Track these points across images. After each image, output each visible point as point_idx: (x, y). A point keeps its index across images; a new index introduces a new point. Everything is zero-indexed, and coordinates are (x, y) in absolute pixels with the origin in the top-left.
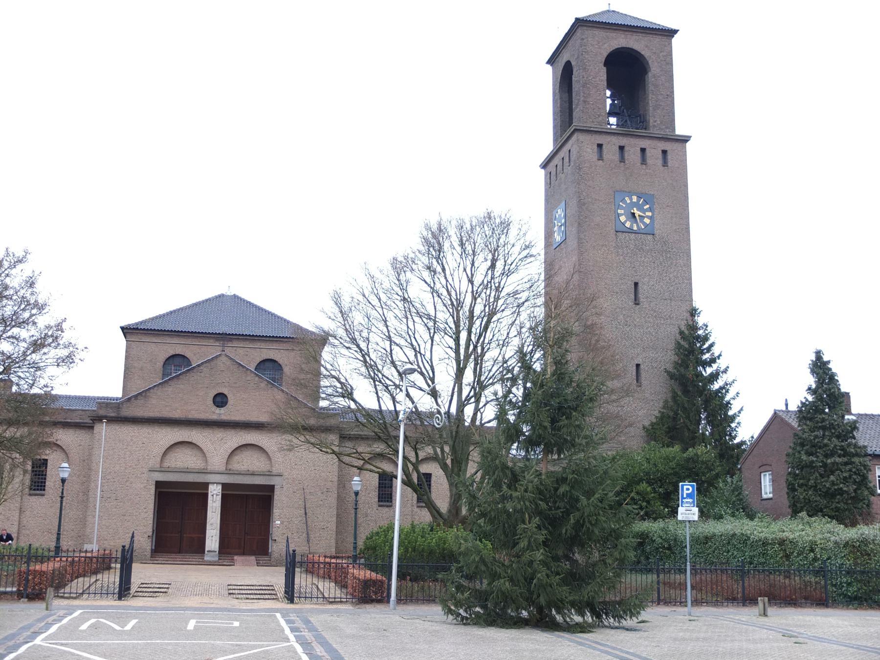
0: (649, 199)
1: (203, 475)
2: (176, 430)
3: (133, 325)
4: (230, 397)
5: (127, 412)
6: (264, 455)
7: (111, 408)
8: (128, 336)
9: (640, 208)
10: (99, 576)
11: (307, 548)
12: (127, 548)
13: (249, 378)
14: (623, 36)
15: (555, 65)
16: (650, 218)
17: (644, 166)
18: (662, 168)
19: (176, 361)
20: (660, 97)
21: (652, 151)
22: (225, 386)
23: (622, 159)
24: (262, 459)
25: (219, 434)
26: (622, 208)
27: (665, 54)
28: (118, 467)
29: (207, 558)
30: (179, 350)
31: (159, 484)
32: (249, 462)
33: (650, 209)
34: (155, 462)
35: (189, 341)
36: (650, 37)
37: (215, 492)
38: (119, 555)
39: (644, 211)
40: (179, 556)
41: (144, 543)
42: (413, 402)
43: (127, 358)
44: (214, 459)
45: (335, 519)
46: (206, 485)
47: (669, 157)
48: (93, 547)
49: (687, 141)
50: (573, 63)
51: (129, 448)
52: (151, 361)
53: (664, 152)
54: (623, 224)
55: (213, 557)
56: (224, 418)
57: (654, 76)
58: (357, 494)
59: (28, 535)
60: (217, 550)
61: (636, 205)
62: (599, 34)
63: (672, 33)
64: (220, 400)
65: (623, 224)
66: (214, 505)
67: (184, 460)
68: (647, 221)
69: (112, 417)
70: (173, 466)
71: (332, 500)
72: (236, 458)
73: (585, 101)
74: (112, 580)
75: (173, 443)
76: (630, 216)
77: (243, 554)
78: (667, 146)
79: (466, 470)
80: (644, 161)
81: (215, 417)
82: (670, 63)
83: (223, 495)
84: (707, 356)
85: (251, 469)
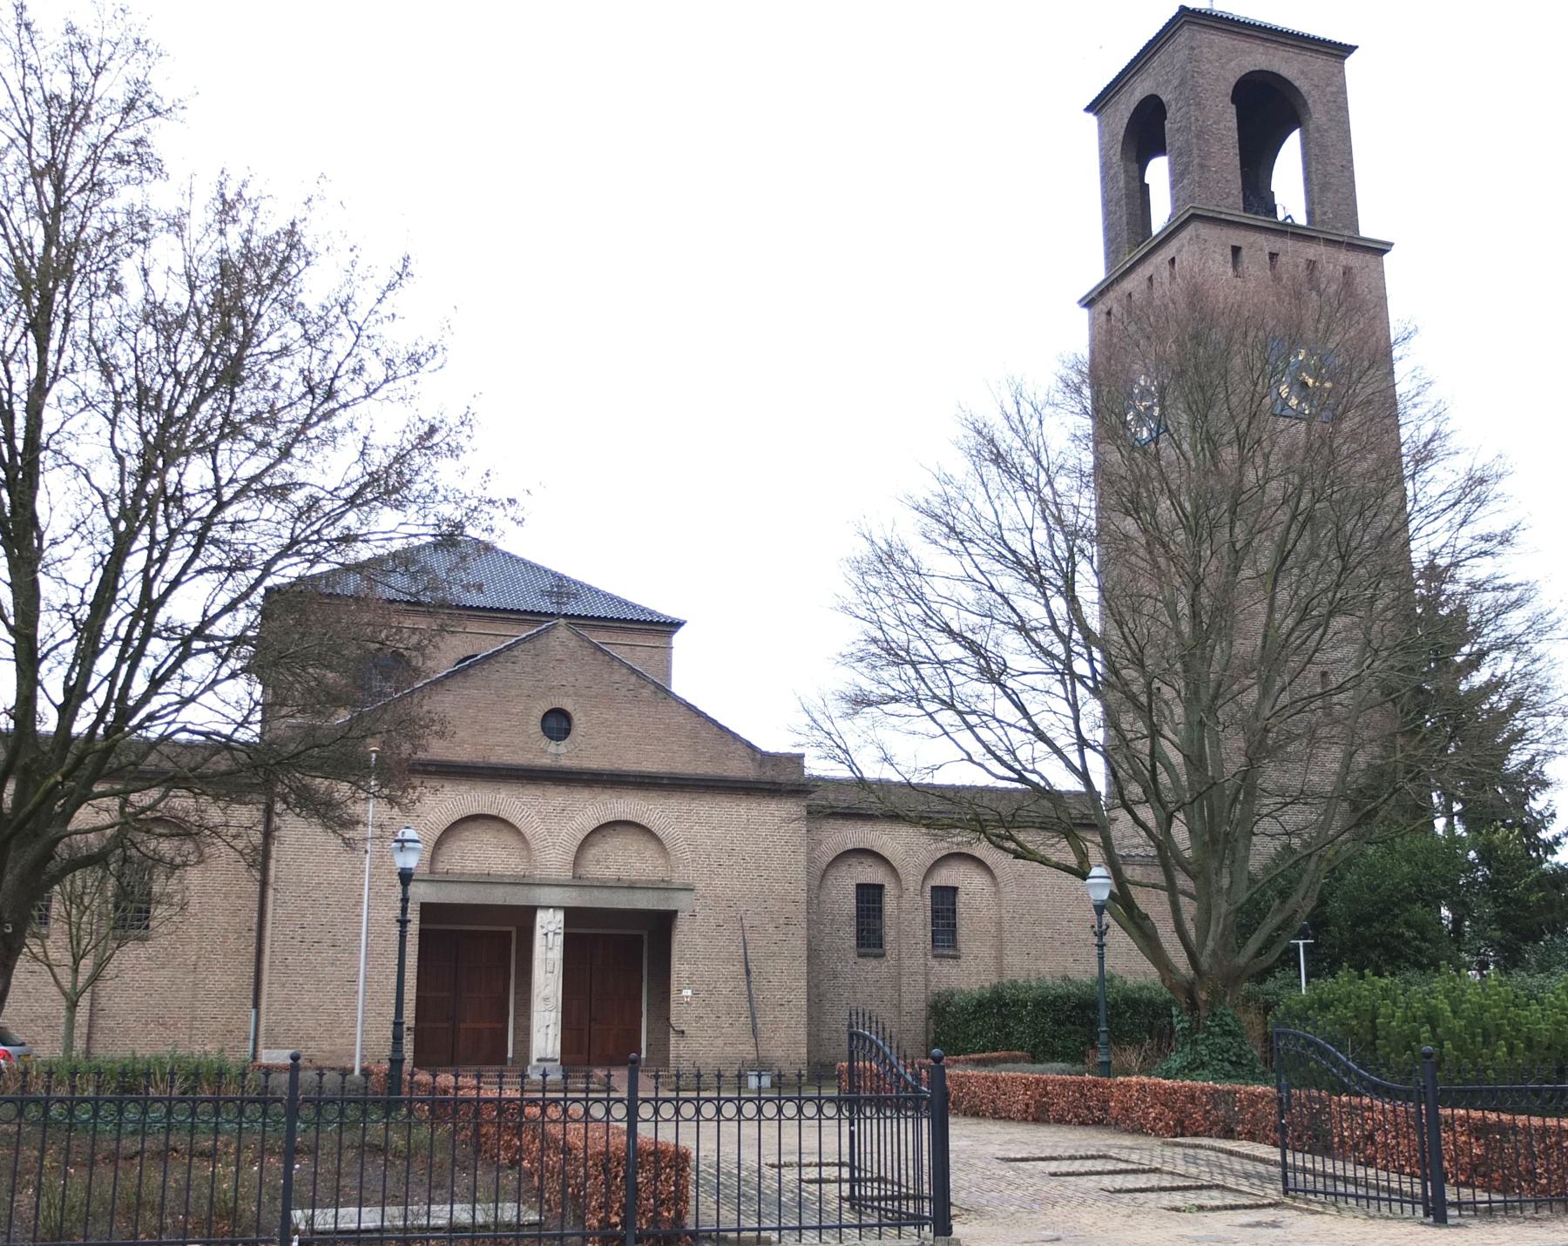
4: (579, 719)
6: (652, 846)
13: (616, 677)
14: (1261, 49)
15: (1109, 111)
22: (567, 695)
24: (647, 854)
25: (557, 798)
27: (1334, 89)
32: (622, 860)
37: (552, 927)
45: (803, 983)
46: (530, 912)
56: (565, 762)
57: (1318, 129)
59: (111, 1029)
60: (558, 1056)
62: (1221, 41)
63: (1350, 49)
64: (557, 724)
66: (550, 955)
67: (482, 855)
70: (457, 869)
71: (799, 945)
72: (593, 853)
73: (1202, 166)
75: (457, 817)
79: (1246, 859)
81: (546, 761)
85: (624, 875)
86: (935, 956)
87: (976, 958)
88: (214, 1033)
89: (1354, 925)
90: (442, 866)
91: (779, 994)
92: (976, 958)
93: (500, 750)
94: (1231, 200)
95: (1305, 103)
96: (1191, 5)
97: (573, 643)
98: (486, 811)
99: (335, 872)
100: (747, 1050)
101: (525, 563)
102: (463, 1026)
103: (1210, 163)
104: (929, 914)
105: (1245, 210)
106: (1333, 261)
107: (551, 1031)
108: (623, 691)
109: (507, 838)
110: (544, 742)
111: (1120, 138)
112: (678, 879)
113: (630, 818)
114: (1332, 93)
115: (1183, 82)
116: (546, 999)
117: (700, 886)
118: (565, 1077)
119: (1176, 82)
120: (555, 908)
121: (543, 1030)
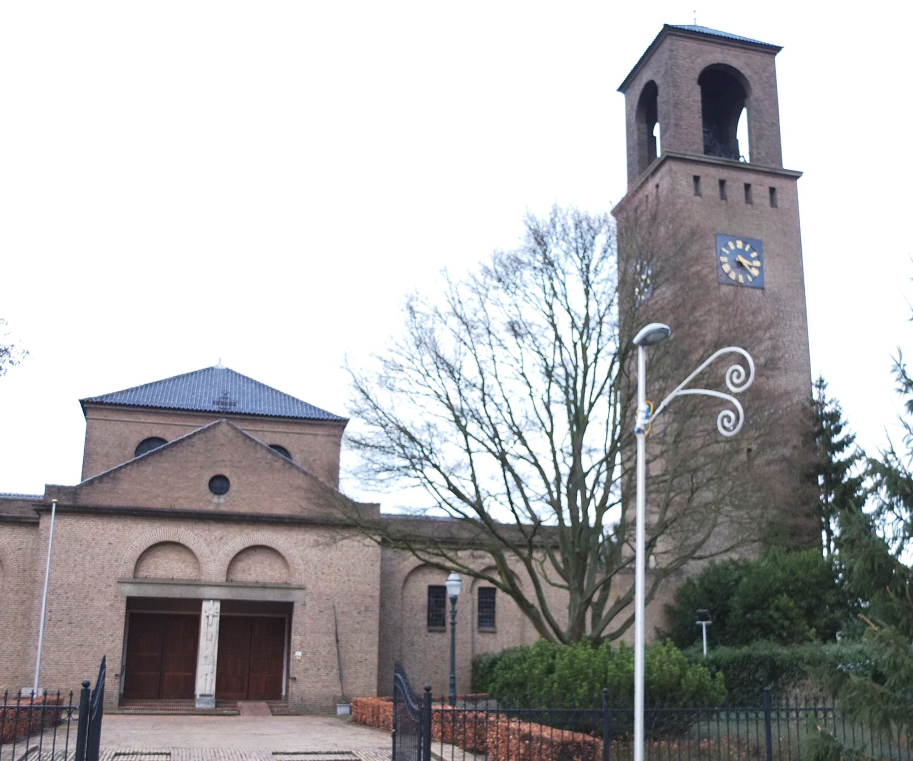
0: (757, 245)
1: (194, 589)
2: (156, 525)
3: (96, 398)
4: (233, 480)
5: (86, 500)
6: (279, 561)
7: (65, 494)
8: (89, 413)
9: (747, 256)
10: (34, 742)
11: (338, 689)
12: (92, 687)
13: (258, 455)
14: (719, 50)
15: (629, 90)
16: (760, 269)
17: (749, 206)
18: (770, 208)
19: (150, 446)
20: (764, 125)
21: (759, 188)
22: (225, 466)
23: (723, 196)
25: (217, 531)
26: (725, 255)
27: (767, 74)
28: (73, 577)
29: (198, 705)
30: (157, 432)
31: (132, 602)
32: (258, 570)
33: (758, 258)
34: (126, 569)
35: (170, 420)
36: (750, 54)
37: (212, 612)
38: (76, 703)
39: (751, 260)
40: (158, 703)
41: (113, 687)
42: (505, 476)
43: (87, 440)
44: (208, 565)
46: (197, 604)
47: (778, 196)
48: (35, 690)
49: (798, 177)
50: (658, 82)
51: (90, 550)
52: (119, 445)
53: (772, 190)
54: (727, 274)
55: (208, 703)
56: (224, 509)
57: (756, 100)
58: (454, 600)
61: (742, 252)
63: (778, 49)
64: (219, 484)
65: (727, 274)
66: (210, 629)
67: (168, 567)
68: (755, 272)
69: (65, 506)
70: (152, 575)
71: (374, 624)
72: (241, 565)
73: (676, 125)
74: (60, 747)
75: (152, 543)
76: (735, 264)
77: (247, 698)
78: (776, 182)
80: (748, 199)
81: (211, 508)
82: (774, 86)
83: (221, 617)
84: (836, 439)
85: (261, 579)
86: (480, 632)
87: (507, 633)
88: (6, 678)
89: (745, 613)
90: (143, 573)
91: (359, 655)
92: (507, 633)
93: (181, 501)
94: (695, 147)
95: (748, 84)
96: (670, 23)
97: (231, 434)
98: (171, 539)
99: (73, 577)
100: (336, 690)
101: (256, 382)
102: (166, 674)
103: (681, 123)
104: (476, 604)
105: (705, 153)
106: (761, 185)
107: (209, 677)
108: (263, 464)
109: (185, 556)
110: (210, 496)
111: (635, 108)
112: (294, 582)
113: (265, 543)
114: (767, 77)
115: (666, 72)
116: (206, 657)
117: (309, 586)
118: (217, 706)
119: (663, 72)
120: (214, 600)
121: (204, 677)
